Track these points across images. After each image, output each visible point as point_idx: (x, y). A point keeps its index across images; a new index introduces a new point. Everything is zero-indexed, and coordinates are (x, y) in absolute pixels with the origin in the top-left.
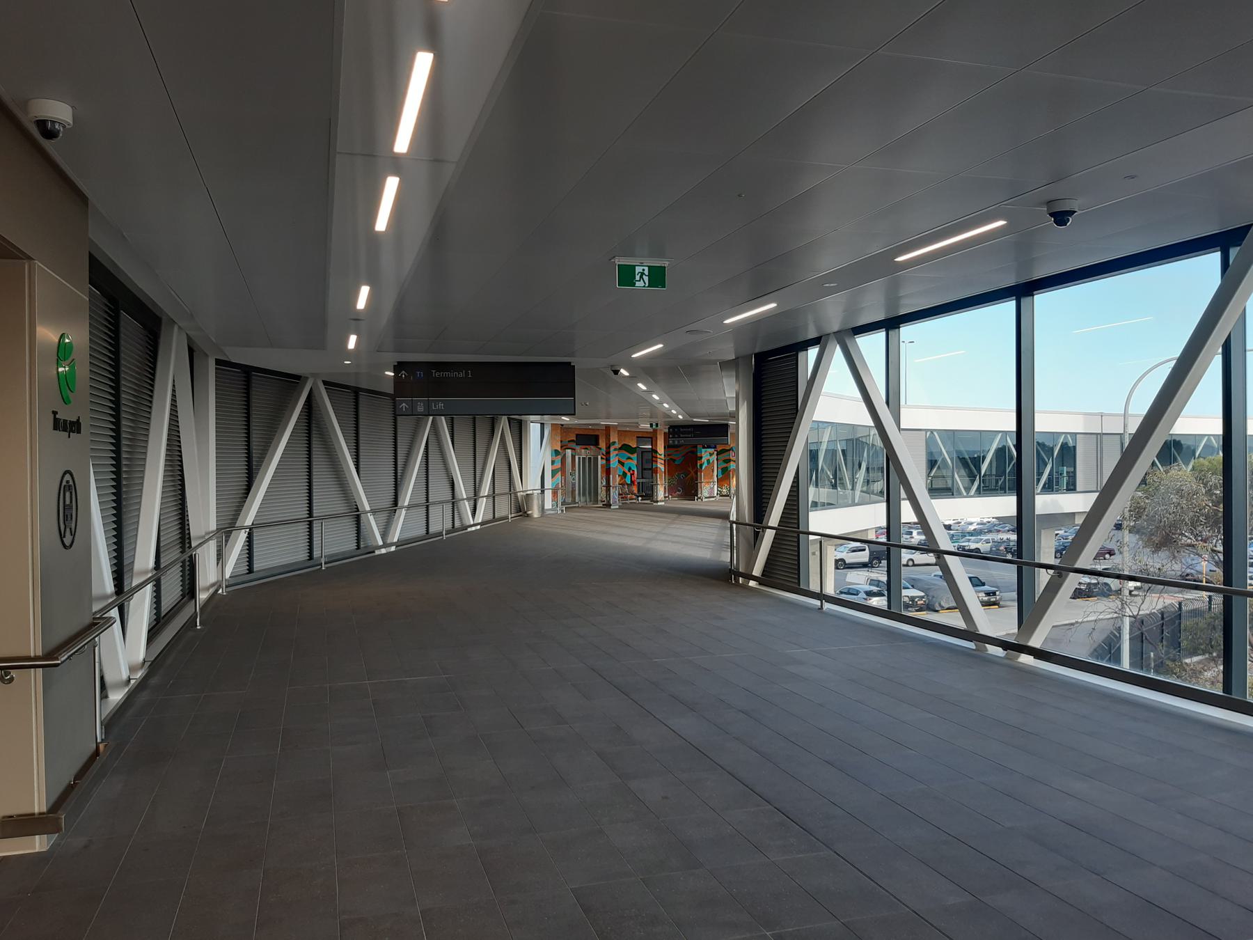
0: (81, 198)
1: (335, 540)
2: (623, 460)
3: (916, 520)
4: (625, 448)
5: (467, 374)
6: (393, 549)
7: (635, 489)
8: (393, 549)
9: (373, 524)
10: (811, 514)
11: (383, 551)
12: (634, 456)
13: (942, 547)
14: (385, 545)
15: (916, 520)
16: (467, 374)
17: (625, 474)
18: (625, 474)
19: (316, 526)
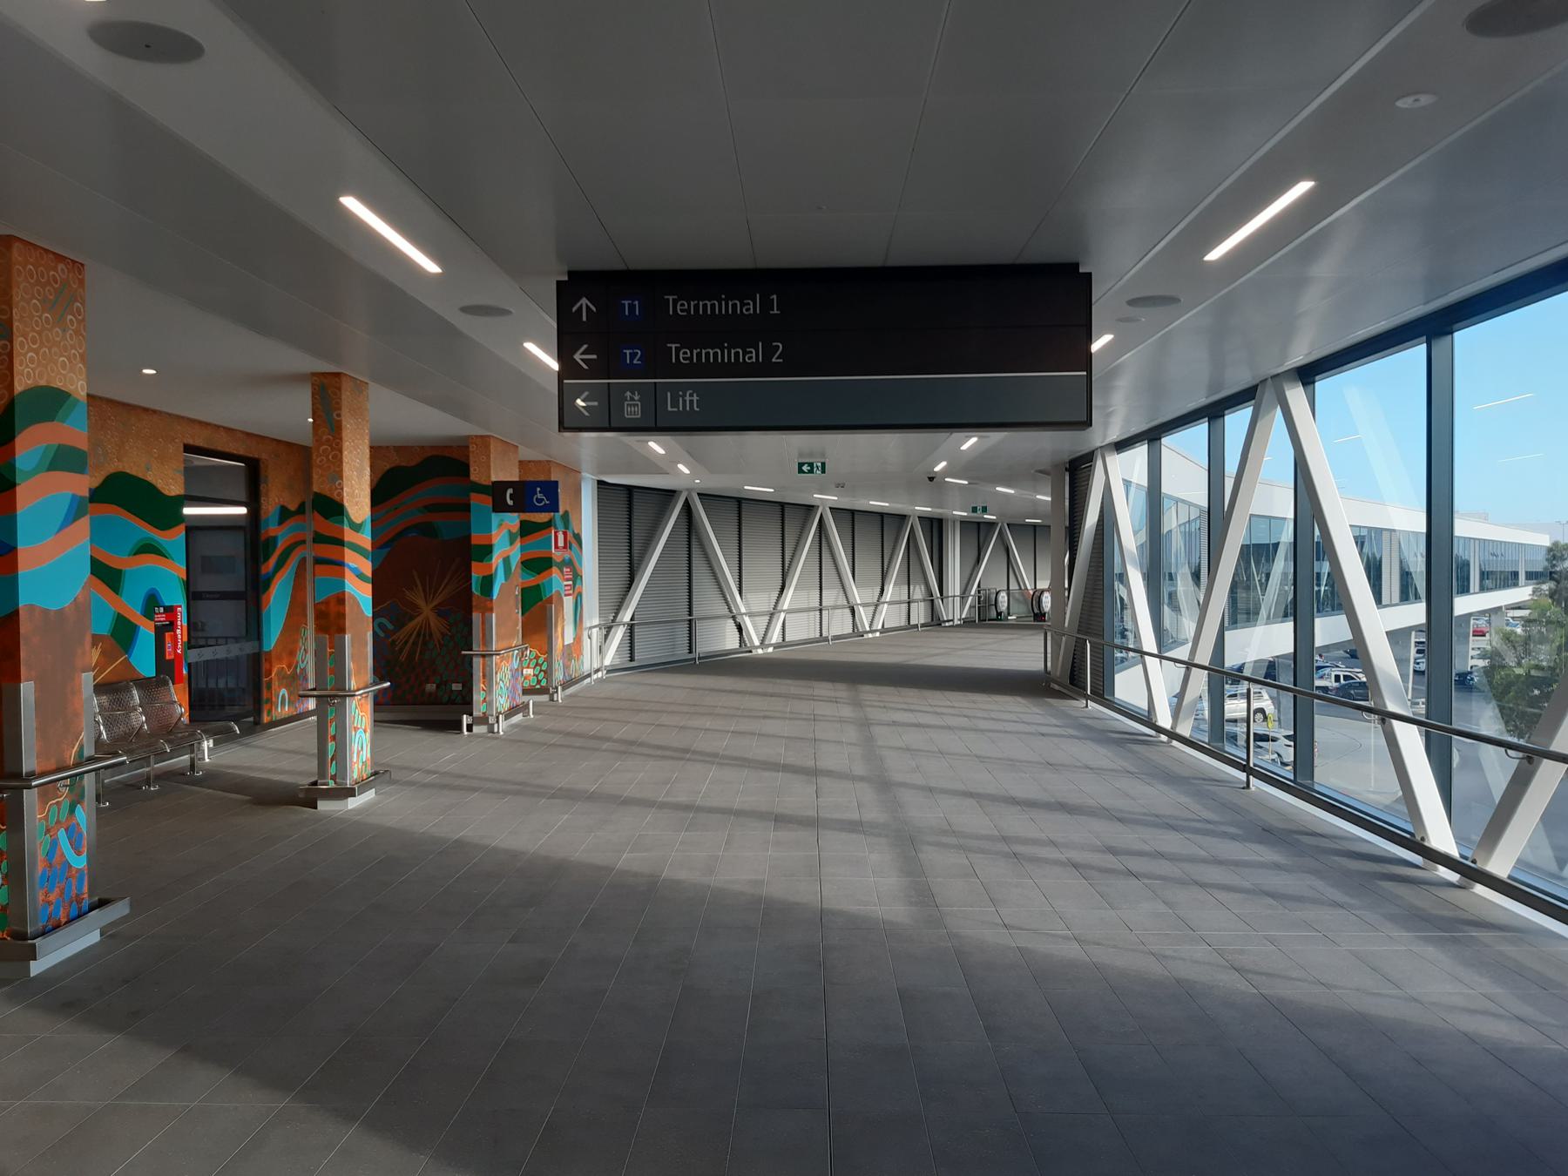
0: (1120, 320)
1: (839, 624)
2: (116, 557)
3: (1422, 349)
4: (123, 494)
5: (766, 305)
6: (770, 650)
7: (178, 702)
8: (770, 650)
9: (864, 614)
10: (1317, 621)
11: (760, 651)
12: (174, 542)
13: (1392, 707)
14: (872, 631)
15: (1422, 349)
16: (766, 305)
17: (124, 634)
18: (124, 634)
19: (825, 613)
